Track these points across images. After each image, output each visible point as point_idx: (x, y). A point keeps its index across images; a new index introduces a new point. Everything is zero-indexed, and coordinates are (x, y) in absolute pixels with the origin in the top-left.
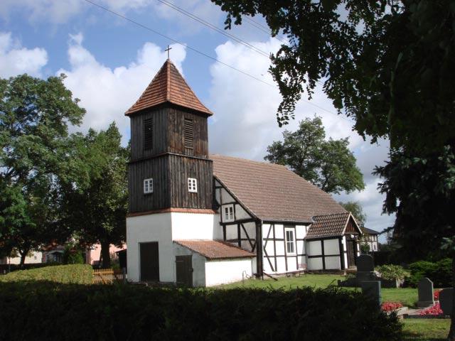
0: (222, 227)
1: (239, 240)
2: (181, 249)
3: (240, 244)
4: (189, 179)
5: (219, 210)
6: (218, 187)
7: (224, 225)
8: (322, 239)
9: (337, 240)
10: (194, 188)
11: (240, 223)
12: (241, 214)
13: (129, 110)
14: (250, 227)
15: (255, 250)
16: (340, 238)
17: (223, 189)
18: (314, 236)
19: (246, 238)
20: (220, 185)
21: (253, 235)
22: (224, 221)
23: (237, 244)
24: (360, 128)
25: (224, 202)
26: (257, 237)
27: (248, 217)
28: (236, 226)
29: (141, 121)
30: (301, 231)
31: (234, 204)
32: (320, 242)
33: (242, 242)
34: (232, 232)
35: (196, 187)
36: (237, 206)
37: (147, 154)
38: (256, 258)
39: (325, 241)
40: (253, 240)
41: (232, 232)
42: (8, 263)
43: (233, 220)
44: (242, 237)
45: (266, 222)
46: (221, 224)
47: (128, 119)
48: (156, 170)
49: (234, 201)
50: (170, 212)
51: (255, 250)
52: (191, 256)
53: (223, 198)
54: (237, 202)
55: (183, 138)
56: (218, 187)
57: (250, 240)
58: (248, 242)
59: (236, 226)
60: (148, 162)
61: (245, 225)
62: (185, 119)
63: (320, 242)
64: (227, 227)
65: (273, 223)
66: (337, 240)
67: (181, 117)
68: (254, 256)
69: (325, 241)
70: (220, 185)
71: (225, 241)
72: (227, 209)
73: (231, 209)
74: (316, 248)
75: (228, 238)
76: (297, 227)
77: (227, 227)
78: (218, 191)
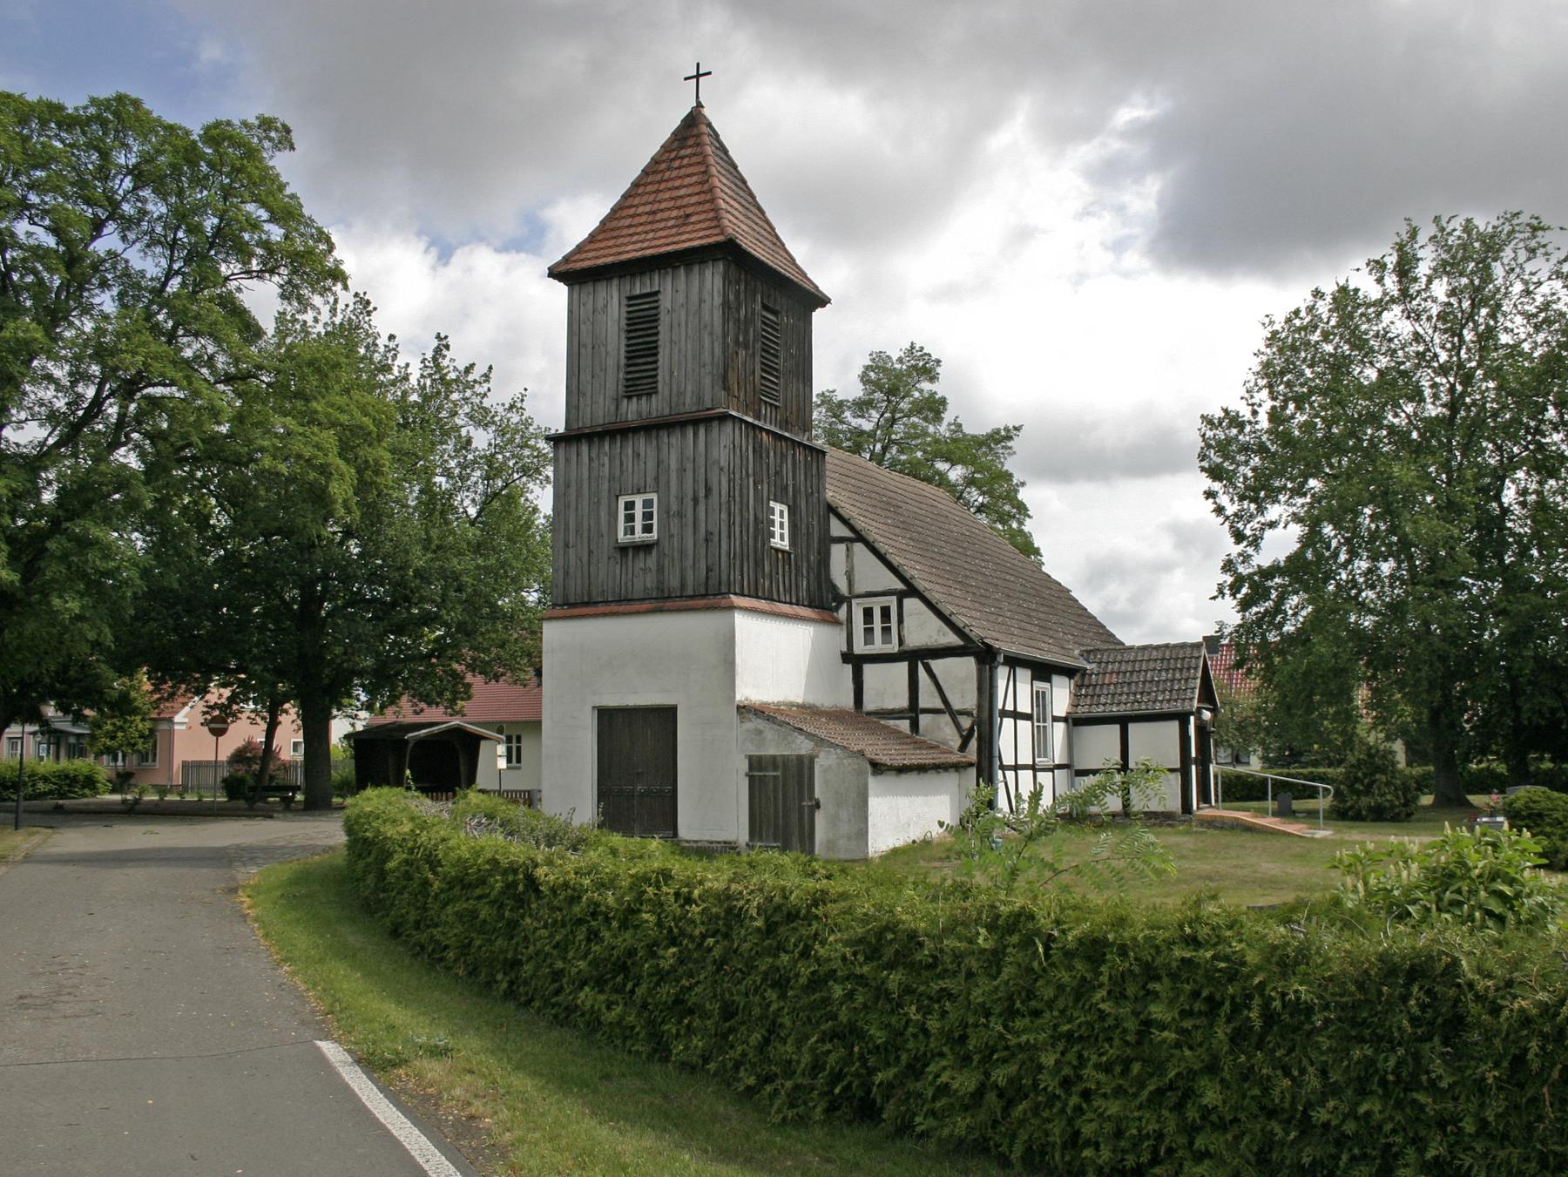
0: (849, 668)
1: (913, 711)
2: (770, 732)
3: (915, 726)
4: (772, 504)
5: (842, 614)
6: (840, 540)
7: (856, 662)
8: (1124, 722)
9: (1174, 726)
10: (782, 538)
11: (916, 657)
12: (922, 629)
13: (566, 259)
14: (959, 674)
15: (973, 744)
16: (1183, 718)
17: (859, 548)
18: (1099, 711)
19: (941, 706)
20: (847, 533)
21: (965, 697)
22: (860, 648)
23: (904, 725)
24: (933, 394)
25: (860, 588)
26: (979, 706)
27: (953, 639)
28: (903, 667)
29: (612, 301)
30: (1061, 696)
31: (901, 595)
32: (1117, 727)
33: (924, 720)
34: (887, 686)
35: (786, 531)
36: (911, 604)
37: (632, 410)
38: (973, 771)
39: (1132, 727)
40: (967, 713)
41: (887, 686)
42: (300, 756)
43: (894, 648)
44: (922, 704)
45: (1014, 662)
46: (848, 657)
47: (561, 290)
48: (674, 465)
49: (900, 586)
50: (732, 607)
51: (973, 744)
52: (812, 759)
53: (857, 577)
54: (911, 591)
55: (758, 372)
56: (840, 540)
57: (954, 715)
58: (947, 717)
59: (903, 667)
60: (641, 442)
61: (937, 665)
62: (765, 307)
63: (1117, 727)
64: (868, 669)
65: (1043, 671)
66: (1174, 726)
67: (755, 301)
68: (971, 765)
69: (1132, 727)
70: (847, 533)
71: (859, 714)
72: (868, 613)
73: (886, 612)
74: (1101, 745)
75: (870, 704)
76: (1055, 678)
77: (868, 669)
78: (838, 552)
